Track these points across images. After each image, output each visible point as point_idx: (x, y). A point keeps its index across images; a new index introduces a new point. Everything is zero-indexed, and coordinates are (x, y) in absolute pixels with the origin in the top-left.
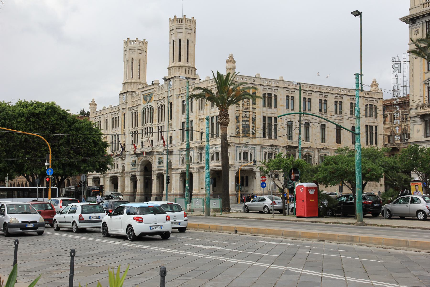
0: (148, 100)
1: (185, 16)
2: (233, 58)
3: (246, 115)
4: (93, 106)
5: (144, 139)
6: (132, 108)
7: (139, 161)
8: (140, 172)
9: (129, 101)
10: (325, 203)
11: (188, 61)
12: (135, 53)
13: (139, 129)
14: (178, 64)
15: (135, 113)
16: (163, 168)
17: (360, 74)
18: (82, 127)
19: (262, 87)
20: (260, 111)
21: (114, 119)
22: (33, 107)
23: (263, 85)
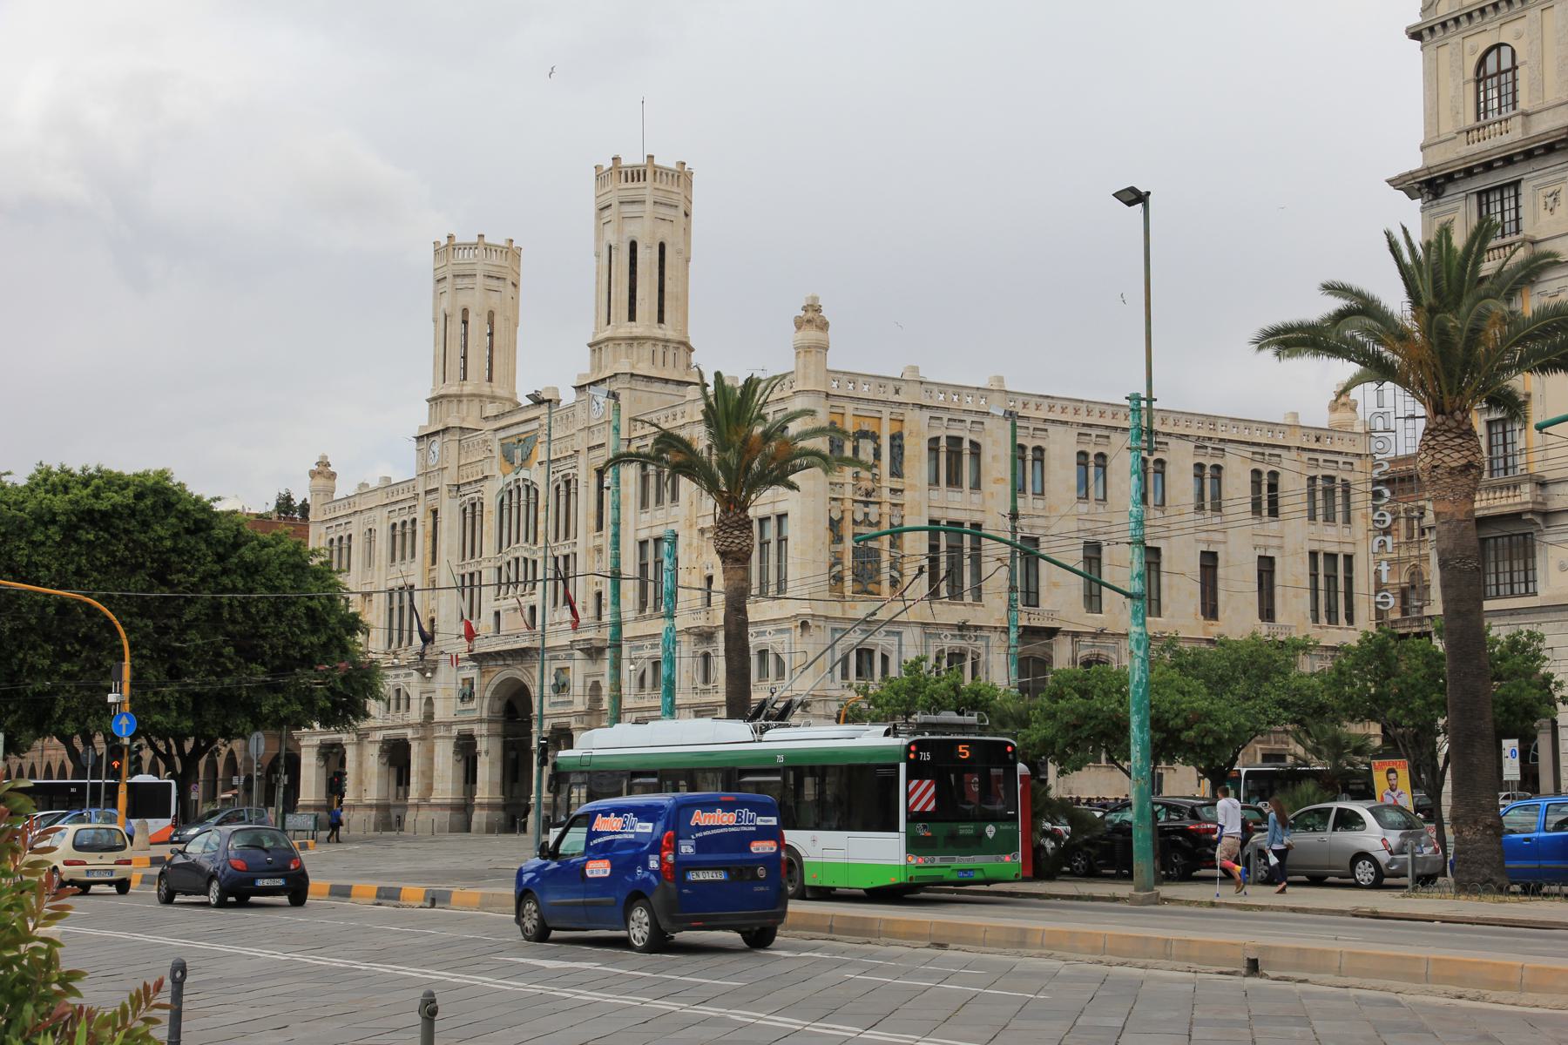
0: (518, 462)
1: (651, 157)
2: (818, 310)
3: (866, 515)
4: (320, 481)
5: (502, 602)
6: (463, 490)
7: (487, 683)
8: (490, 721)
9: (452, 464)
10: (1064, 828)
11: (661, 320)
12: (476, 289)
13: (484, 564)
14: (626, 329)
15: (474, 505)
16: (569, 709)
17: (1144, 395)
18: (268, 563)
19: (927, 414)
20: (921, 499)
21: (399, 528)
22: (89, 490)
23: (928, 407)
